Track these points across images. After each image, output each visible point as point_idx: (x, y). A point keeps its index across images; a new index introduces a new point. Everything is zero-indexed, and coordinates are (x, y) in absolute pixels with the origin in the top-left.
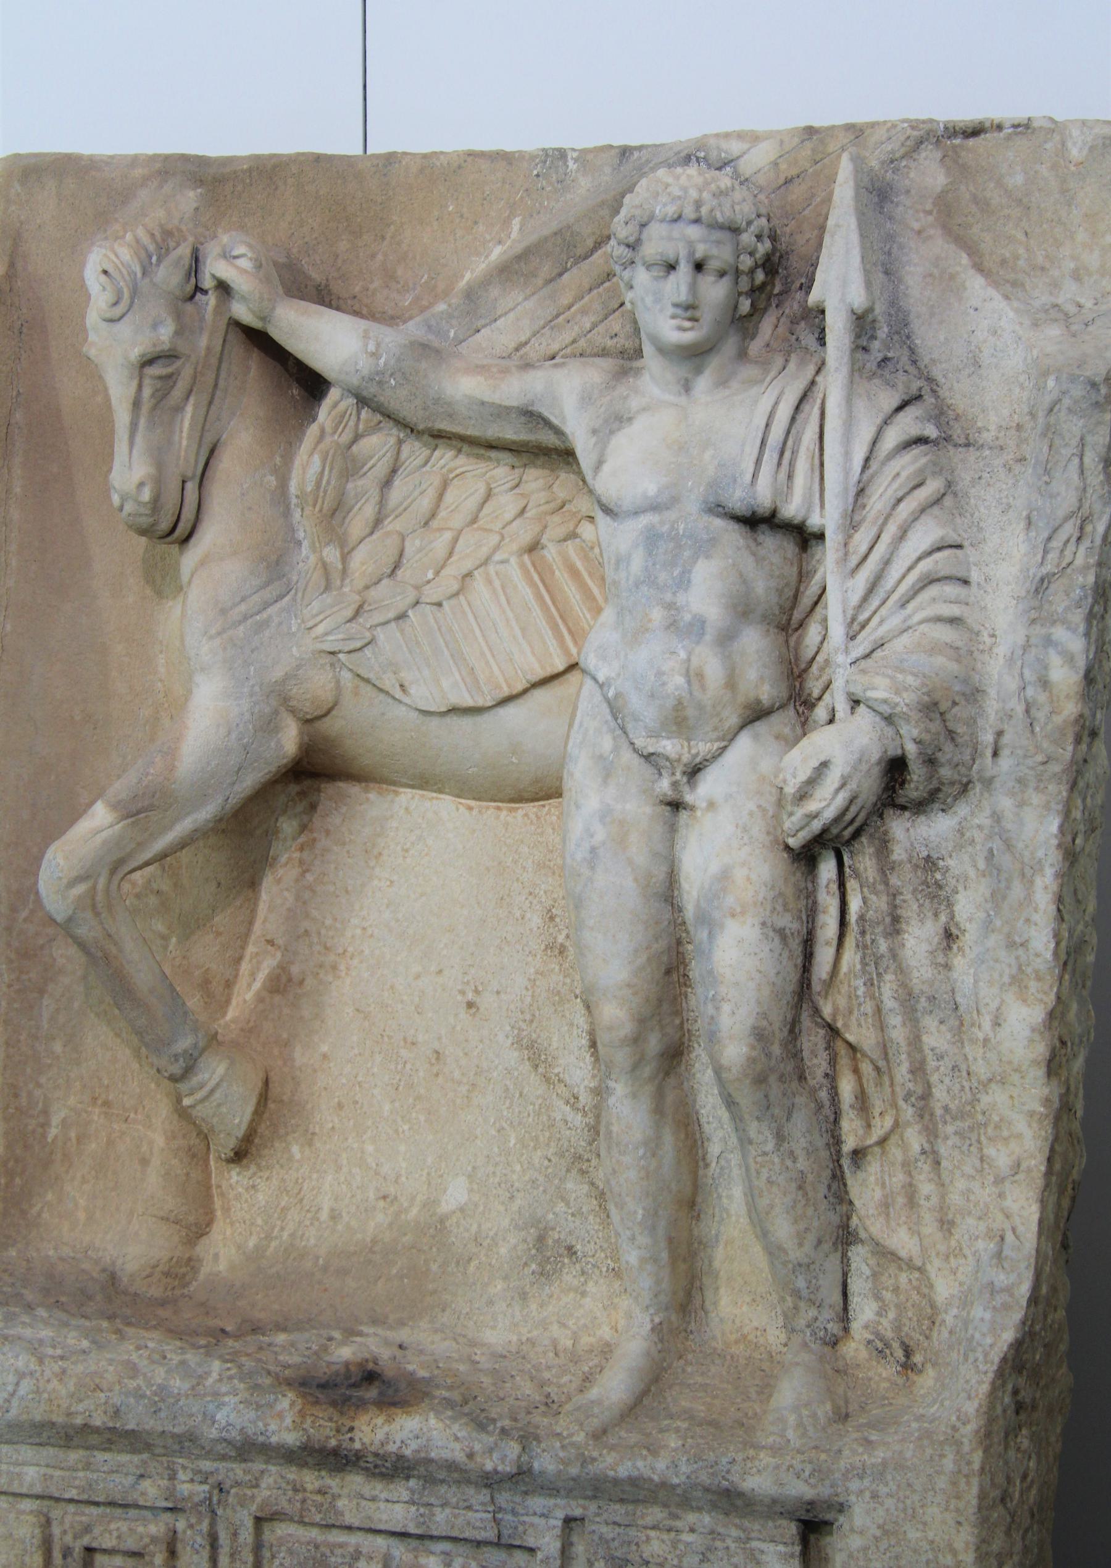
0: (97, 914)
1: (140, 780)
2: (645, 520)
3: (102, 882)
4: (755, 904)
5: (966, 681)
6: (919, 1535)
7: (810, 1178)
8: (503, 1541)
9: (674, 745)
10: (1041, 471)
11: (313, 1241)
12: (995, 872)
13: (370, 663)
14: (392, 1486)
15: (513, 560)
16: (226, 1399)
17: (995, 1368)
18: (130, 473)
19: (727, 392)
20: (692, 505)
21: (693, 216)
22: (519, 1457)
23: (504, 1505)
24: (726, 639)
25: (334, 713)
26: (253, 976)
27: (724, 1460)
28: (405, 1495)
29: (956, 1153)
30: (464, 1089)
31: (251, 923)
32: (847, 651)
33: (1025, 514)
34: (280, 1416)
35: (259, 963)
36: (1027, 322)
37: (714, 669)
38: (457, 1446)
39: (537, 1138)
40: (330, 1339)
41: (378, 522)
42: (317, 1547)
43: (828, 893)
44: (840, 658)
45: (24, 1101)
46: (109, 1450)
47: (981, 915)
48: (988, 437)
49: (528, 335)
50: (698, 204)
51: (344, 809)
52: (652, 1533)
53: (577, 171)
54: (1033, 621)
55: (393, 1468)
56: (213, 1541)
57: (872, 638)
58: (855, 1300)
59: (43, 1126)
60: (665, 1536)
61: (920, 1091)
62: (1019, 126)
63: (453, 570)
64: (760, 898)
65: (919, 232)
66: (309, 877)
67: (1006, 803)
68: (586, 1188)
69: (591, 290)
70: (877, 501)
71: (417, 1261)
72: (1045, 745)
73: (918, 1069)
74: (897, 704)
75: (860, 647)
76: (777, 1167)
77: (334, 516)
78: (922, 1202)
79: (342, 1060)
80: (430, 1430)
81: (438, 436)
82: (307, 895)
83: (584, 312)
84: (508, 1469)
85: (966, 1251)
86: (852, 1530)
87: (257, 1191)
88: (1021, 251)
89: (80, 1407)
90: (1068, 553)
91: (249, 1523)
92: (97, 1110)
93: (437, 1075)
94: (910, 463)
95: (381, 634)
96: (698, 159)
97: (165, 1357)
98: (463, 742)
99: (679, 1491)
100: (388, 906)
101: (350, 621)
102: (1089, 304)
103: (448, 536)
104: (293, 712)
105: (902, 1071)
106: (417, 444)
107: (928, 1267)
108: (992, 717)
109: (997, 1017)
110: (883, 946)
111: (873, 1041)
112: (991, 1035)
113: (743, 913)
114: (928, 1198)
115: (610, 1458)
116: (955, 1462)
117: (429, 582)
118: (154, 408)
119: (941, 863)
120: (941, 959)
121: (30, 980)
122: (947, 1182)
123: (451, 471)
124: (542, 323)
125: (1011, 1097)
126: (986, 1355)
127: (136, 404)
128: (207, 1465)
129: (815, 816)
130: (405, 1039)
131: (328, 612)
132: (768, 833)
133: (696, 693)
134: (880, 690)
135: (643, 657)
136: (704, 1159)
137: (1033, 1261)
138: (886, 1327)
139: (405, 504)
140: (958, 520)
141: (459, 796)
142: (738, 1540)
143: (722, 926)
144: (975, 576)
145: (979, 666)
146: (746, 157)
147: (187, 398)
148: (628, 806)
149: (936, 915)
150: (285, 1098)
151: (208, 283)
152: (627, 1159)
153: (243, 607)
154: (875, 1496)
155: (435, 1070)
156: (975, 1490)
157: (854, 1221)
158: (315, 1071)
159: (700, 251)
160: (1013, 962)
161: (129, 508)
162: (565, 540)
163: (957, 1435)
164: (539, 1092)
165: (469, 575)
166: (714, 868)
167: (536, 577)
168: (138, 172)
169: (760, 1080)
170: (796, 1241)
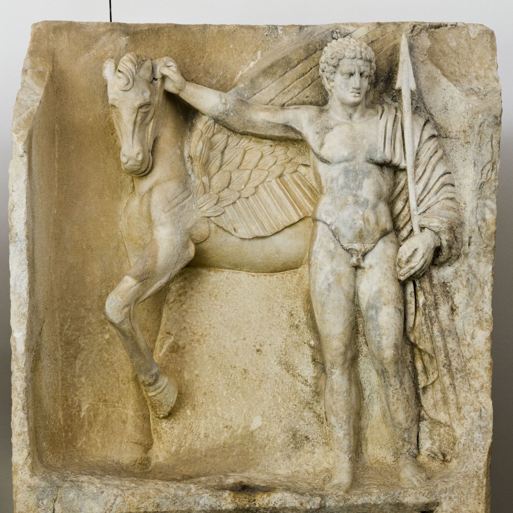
0: (130, 320)
2: (343, 165)
3: (132, 306)
4: (392, 300)
5: (459, 220)
6: (466, 509)
7: (410, 397)
10: (478, 147)
11: (199, 446)
12: (470, 286)
13: (223, 221)
15: (274, 181)
16: (204, 495)
17: (488, 451)
18: (130, 150)
19: (365, 119)
20: (361, 158)
21: (360, 57)
22: (321, 502)
26: (162, 347)
27: (397, 493)
29: (461, 384)
30: (257, 383)
31: (159, 326)
32: (417, 210)
33: (473, 161)
34: (225, 499)
36: (464, 95)
37: (372, 218)
41: (221, 167)
43: (411, 296)
44: (415, 213)
45: (70, 402)
49: (274, 96)
50: (361, 52)
51: (199, 279)
53: (283, 34)
54: (479, 198)
57: (426, 205)
58: (422, 442)
61: (448, 363)
62: (453, 25)
63: (251, 185)
64: (393, 298)
65: (423, 62)
66: (185, 307)
67: (473, 262)
68: (312, 414)
70: (424, 158)
71: (246, 446)
72: (486, 241)
73: (447, 356)
75: (422, 208)
76: (400, 394)
77: (206, 164)
78: (451, 402)
79: (205, 374)
80: (286, 497)
81: (244, 134)
83: (295, 88)
84: (316, 507)
85: (467, 417)
87: (174, 429)
88: (457, 69)
89: (143, 505)
90: (489, 174)
92: (101, 404)
93: (245, 378)
94: (432, 144)
95: (227, 210)
96: (337, 32)
98: (259, 251)
99: (380, 507)
102: (482, 88)
103: (248, 172)
105: (441, 357)
106: (235, 137)
107: (453, 424)
108: (468, 232)
110: (433, 313)
111: (430, 348)
112: (471, 342)
113: (388, 304)
114: (453, 400)
115: (355, 498)
116: (478, 483)
118: (141, 124)
119: (448, 284)
120: (451, 318)
121: (70, 353)
123: (247, 147)
124: (279, 91)
126: (483, 448)
127: (135, 123)
129: (413, 268)
130: (231, 366)
131: (207, 202)
132: (393, 276)
133: (367, 227)
134: (435, 223)
136: (363, 397)
137: (492, 416)
138: (435, 449)
139: (230, 160)
140: (448, 164)
141: (248, 272)
143: (381, 309)
144: (456, 183)
145: (462, 214)
146: (355, 32)
147: (151, 121)
148: (341, 268)
149: (448, 302)
151: (158, 76)
152: (340, 398)
153: (176, 200)
154: (450, 498)
156: (484, 492)
157: (423, 412)
158: (194, 381)
159: (362, 69)
160: (477, 316)
161: (130, 163)
162: (293, 173)
163: (478, 474)
165: (257, 187)
166: (375, 289)
168: (102, 30)
169: (396, 363)
170: (405, 420)
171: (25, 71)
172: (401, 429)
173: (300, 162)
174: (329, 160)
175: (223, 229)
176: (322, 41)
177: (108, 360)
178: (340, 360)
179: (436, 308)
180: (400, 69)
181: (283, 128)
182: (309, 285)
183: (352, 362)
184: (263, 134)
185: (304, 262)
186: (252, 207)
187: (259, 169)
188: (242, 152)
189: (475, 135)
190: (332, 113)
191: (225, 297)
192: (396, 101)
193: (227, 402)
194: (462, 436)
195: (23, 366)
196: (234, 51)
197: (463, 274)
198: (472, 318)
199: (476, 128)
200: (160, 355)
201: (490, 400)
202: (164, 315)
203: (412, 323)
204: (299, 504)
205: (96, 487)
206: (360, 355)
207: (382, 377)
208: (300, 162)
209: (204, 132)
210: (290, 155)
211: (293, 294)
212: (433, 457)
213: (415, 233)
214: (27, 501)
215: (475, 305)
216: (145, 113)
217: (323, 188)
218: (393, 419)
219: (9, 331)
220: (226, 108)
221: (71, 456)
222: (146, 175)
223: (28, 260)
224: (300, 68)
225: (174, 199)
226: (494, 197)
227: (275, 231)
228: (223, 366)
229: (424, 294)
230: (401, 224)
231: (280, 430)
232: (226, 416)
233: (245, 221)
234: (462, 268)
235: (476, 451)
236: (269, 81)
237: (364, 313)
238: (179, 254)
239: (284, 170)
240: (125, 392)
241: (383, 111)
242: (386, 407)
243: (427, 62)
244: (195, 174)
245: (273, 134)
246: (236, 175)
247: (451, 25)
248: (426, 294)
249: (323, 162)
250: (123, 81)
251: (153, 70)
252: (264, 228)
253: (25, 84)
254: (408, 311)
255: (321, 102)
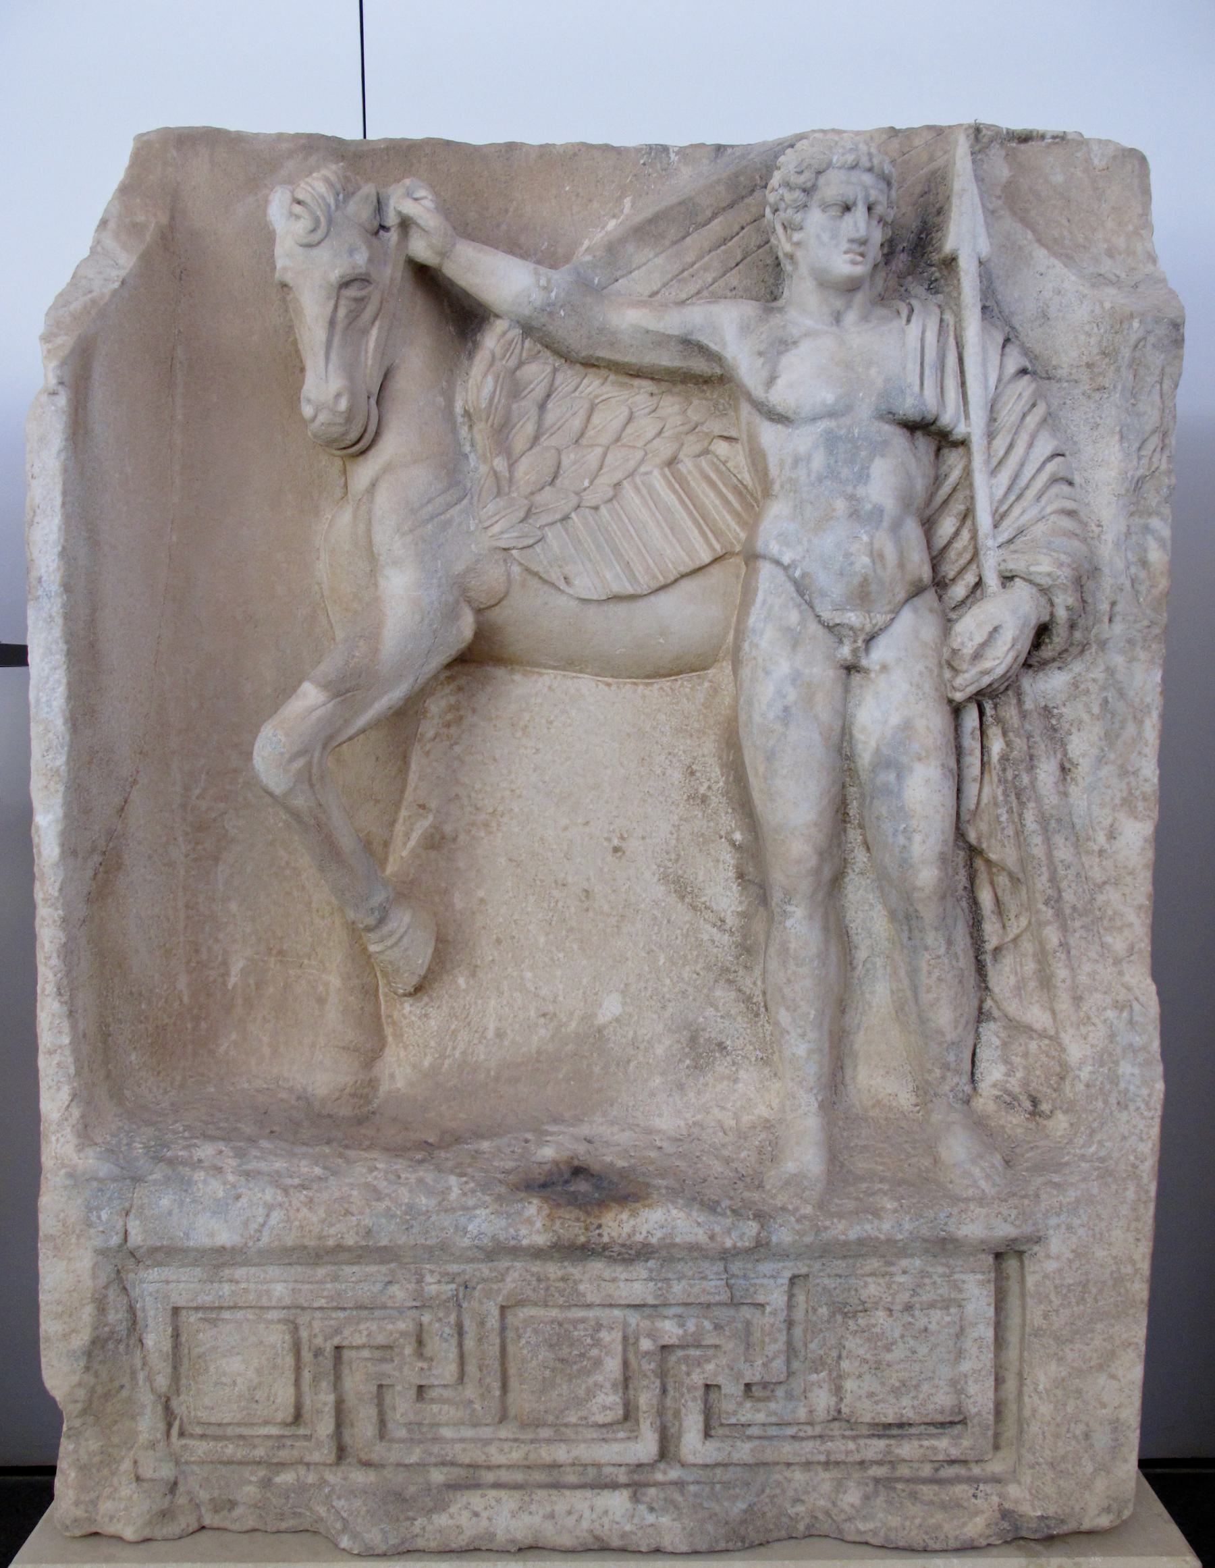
0: (312, 786)
1: (347, 663)
2: (822, 426)
3: (317, 754)
6: (1105, 1253)
7: (966, 973)
8: (735, 1301)
9: (857, 617)
11: (482, 1057)
12: (1109, 716)
14: (631, 1268)
15: (656, 473)
16: (478, 1212)
18: (323, 388)
20: (865, 410)
21: (868, 165)
22: (759, 1234)
23: (736, 1272)
24: (896, 526)
25: (504, 603)
26: (407, 836)
27: (942, 1215)
28: (644, 1274)
30: (613, 920)
31: (402, 791)
32: (994, 537)
33: (1118, 429)
34: (529, 1221)
35: (412, 824)
38: (701, 1231)
39: (685, 956)
40: (527, 1141)
41: (536, 439)
42: (560, 1324)
43: (973, 738)
45: (204, 956)
46: (359, 1263)
47: (1095, 751)
48: (1062, 373)
49: (659, 285)
50: (870, 155)
51: (489, 689)
52: (869, 1280)
53: (679, 161)
54: (1132, 514)
55: (635, 1254)
56: (460, 1330)
57: (1015, 526)
58: (982, 1066)
59: (223, 975)
60: (881, 1281)
63: (605, 480)
67: (1118, 660)
68: (733, 995)
69: (710, 251)
71: (583, 1064)
72: (1148, 612)
73: (1053, 879)
74: (1059, 577)
76: (946, 968)
77: (502, 431)
78: (1059, 984)
79: (499, 900)
80: (674, 1219)
81: (590, 364)
82: (456, 764)
83: (706, 269)
86: (1048, 1256)
88: (1066, 233)
89: (332, 1231)
91: (496, 1312)
92: (272, 960)
93: (587, 910)
97: (399, 1177)
100: (535, 770)
101: (521, 521)
102: (1123, 275)
103: (599, 451)
104: (469, 602)
105: (1042, 882)
106: (570, 372)
107: (1062, 1035)
108: (1108, 590)
109: (1111, 832)
112: (1107, 846)
113: (927, 757)
114: (1064, 981)
115: (841, 1225)
116: (1137, 1193)
117: (585, 489)
119: (1055, 711)
120: (1061, 789)
121: (204, 849)
122: (1076, 966)
123: (597, 397)
124: (670, 276)
125: (1124, 895)
126: (1147, 1104)
127: (332, 323)
128: (454, 1268)
130: (556, 882)
131: (503, 514)
132: (936, 689)
134: (1043, 566)
135: (828, 542)
138: (1014, 1084)
142: (942, 1276)
143: (911, 770)
144: (1077, 479)
147: (373, 323)
148: (815, 670)
150: (450, 938)
151: (392, 220)
152: (804, 970)
153: (430, 508)
154: (1069, 1228)
155: (585, 905)
157: (989, 1003)
158: (473, 913)
159: (874, 195)
160: (1124, 785)
161: (322, 418)
162: (699, 456)
163: (1138, 1172)
164: (687, 918)
165: (618, 485)
166: (895, 720)
167: (677, 486)
168: (285, 146)
169: (943, 898)
171: (104, 223)
172: (940, 1044)
173: (717, 433)
174: (790, 414)
175: (540, 578)
176: (767, 167)
177: (287, 863)
178: (805, 886)
179: (1031, 768)
180: (954, 209)
181: (680, 347)
182: (735, 708)
183: (832, 884)
184: (634, 361)
185: (721, 655)
186: (607, 530)
187: (623, 446)
188: (586, 405)
189: (1123, 369)
190: (793, 314)
191: (545, 731)
192: (937, 292)
193: (547, 960)
194: (1082, 1063)
195: (56, 894)
196: (574, 198)
197: (1094, 688)
198: (1110, 791)
199: (1126, 353)
200: (404, 854)
201: (1149, 981)
202: (414, 766)
203: (974, 801)
204: (706, 1237)
205: (225, 1184)
206: (850, 871)
207: (905, 928)
208: (717, 430)
209: (498, 356)
210: (694, 416)
211: (696, 725)
212: (1008, 1101)
213: (990, 590)
214: (63, 1211)
215: (1119, 762)
216: (355, 300)
217: (772, 483)
218: (923, 1020)
219: (27, 813)
220: (549, 297)
221: (203, 1075)
222: (363, 452)
223: (67, 642)
224: (717, 227)
225: (423, 506)
226: (1166, 510)
227: (658, 585)
228: (538, 882)
229: (1005, 734)
230: (949, 570)
231: (661, 1026)
232: (544, 992)
233: (590, 560)
234: (1092, 675)
235: (1126, 1107)
236: (648, 253)
237: (864, 776)
238: (435, 631)
239: (679, 449)
240: (325, 935)
241: (912, 310)
242: (909, 994)
243: (1002, 212)
244: (475, 451)
245: (657, 362)
246: (572, 456)
247: (1054, 137)
248: (1011, 734)
249: (772, 420)
250: (301, 227)
251: (380, 206)
252: (633, 578)
253: (99, 249)
254: (965, 772)
255: (767, 279)
